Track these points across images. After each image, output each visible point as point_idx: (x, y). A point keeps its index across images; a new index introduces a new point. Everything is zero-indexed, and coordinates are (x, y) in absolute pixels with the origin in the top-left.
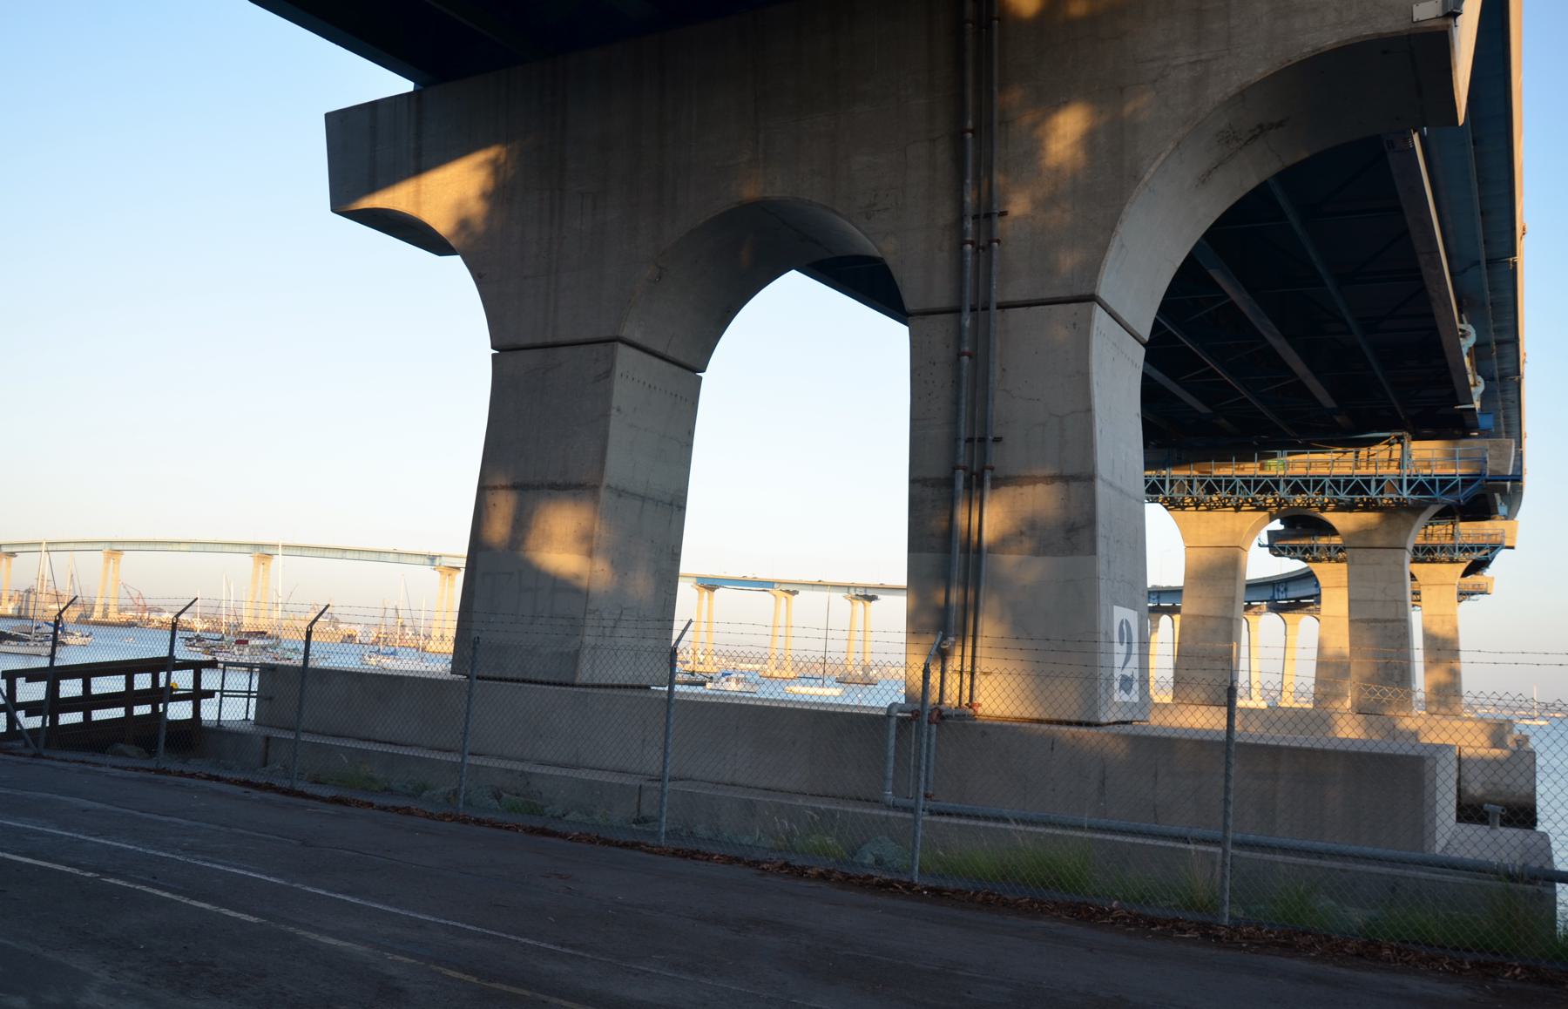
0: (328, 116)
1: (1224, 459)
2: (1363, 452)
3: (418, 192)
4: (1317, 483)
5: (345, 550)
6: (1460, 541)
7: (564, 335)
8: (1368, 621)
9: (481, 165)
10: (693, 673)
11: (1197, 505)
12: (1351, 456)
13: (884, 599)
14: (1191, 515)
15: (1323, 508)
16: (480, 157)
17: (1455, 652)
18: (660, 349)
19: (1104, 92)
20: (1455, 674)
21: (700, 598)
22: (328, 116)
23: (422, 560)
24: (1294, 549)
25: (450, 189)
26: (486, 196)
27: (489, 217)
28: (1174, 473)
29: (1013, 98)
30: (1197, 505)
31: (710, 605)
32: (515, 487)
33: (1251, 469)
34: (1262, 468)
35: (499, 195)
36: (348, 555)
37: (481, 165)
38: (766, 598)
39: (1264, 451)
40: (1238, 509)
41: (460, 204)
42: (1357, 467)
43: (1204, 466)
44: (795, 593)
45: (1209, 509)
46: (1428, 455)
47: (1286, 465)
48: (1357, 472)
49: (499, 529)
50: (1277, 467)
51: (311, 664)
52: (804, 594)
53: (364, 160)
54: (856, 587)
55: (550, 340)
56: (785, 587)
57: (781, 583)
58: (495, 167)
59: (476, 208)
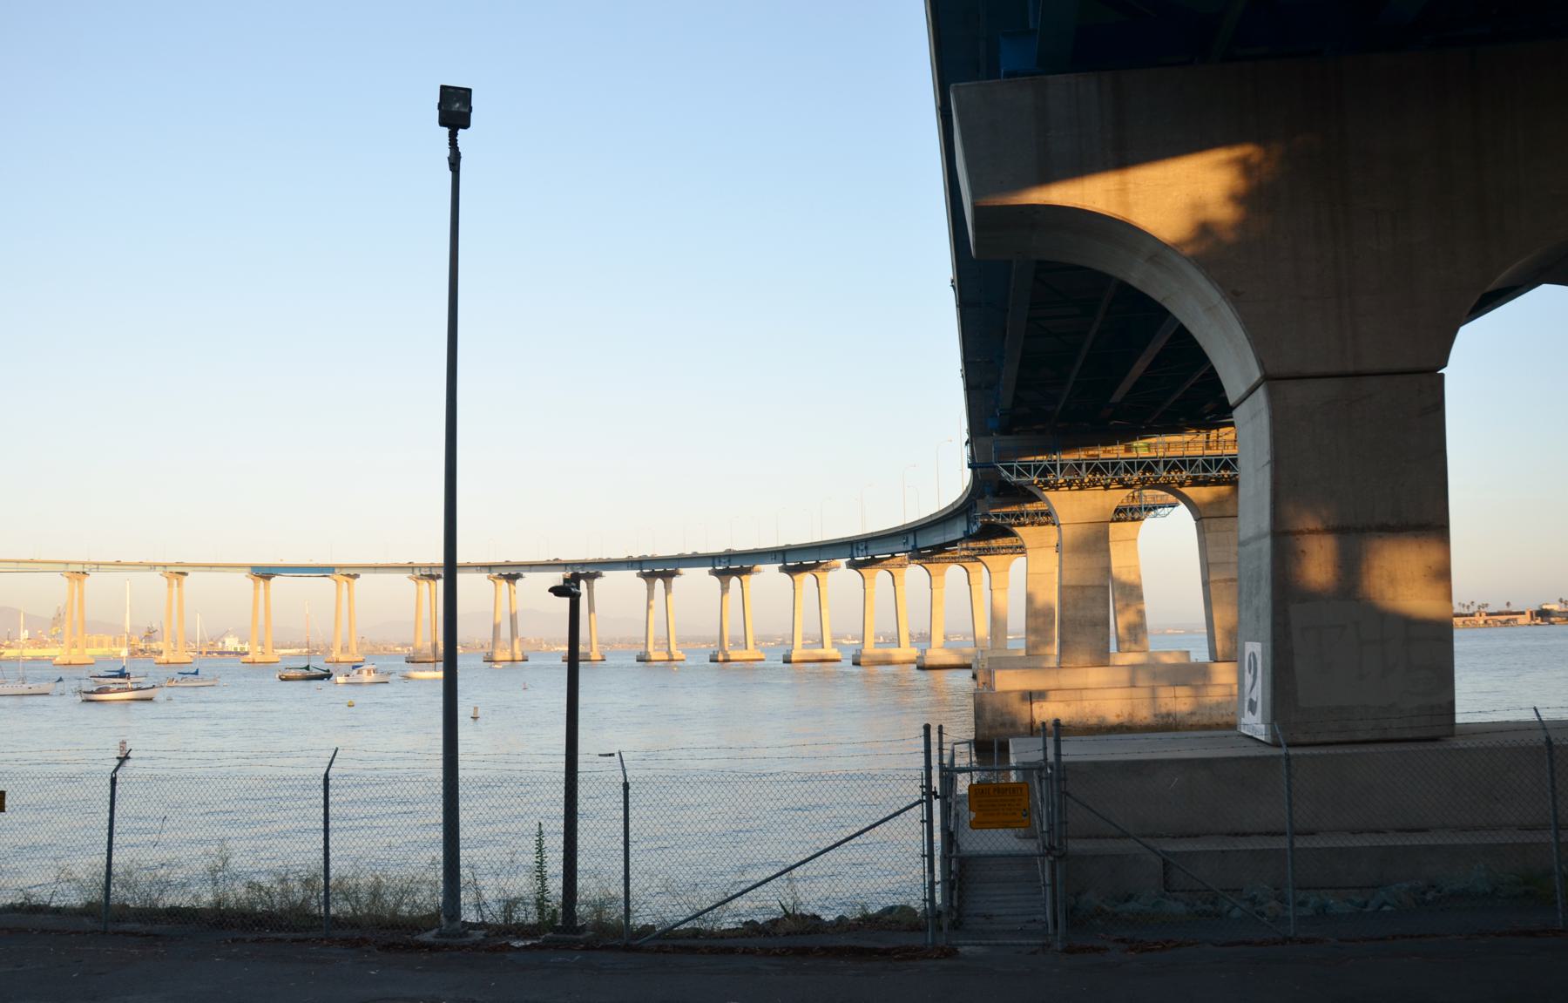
0: (469, 91)
1: (1109, 442)
2: (1214, 433)
3: (1123, 190)
8: (1225, 581)
9: (1230, 162)
10: (307, 668)
11: (1070, 486)
12: (1203, 437)
15: (1181, 484)
17: (1140, 597)
20: (1141, 613)
21: (256, 588)
22: (469, 91)
26: (1236, 198)
27: (1242, 226)
30: (1070, 486)
31: (266, 594)
32: (1329, 530)
33: (1117, 452)
34: (1128, 450)
35: (1254, 198)
37: (1230, 162)
38: (326, 584)
39: (1127, 435)
40: (1107, 487)
41: (1196, 206)
42: (1208, 447)
44: (356, 576)
45: (1081, 488)
48: (1207, 452)
50: (1142, 449)
51: (1063, 759)
52: (365, 577)
54: (420, 568)
55: (1351, 368)
56: (345, 572)
57: (341, 567)
59: (1223, 213)
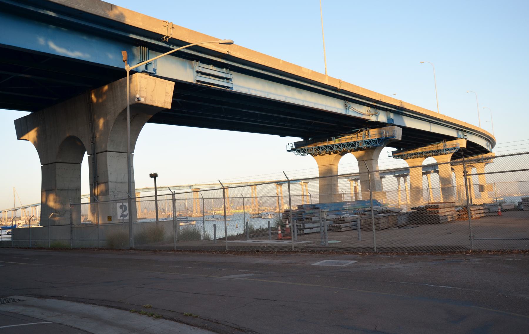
4: (343, 145)
5: (162, 188)
6: (447, 147)
7: (50, 162)
8: (365, 181)
10: (258, 214)
12: (356, 136)
13: (311, 182)
14: (318, 157)
16: (35, 129)
18: (67, 162)
19: (105, 116)
23: (166, 189)
24: (398, 156)
25: (32, 134)
28: (308, 147)
29: (95, 116)
31: (281, 190)
33: (326, 144)
36: (163, 189)
40: (330, 154)
43: (315, 144)
44: (308, 182)
46: (375, 133)
47: (346, 139)
49: (44, 200)
53: (22, 129)
58: (38, 132)
